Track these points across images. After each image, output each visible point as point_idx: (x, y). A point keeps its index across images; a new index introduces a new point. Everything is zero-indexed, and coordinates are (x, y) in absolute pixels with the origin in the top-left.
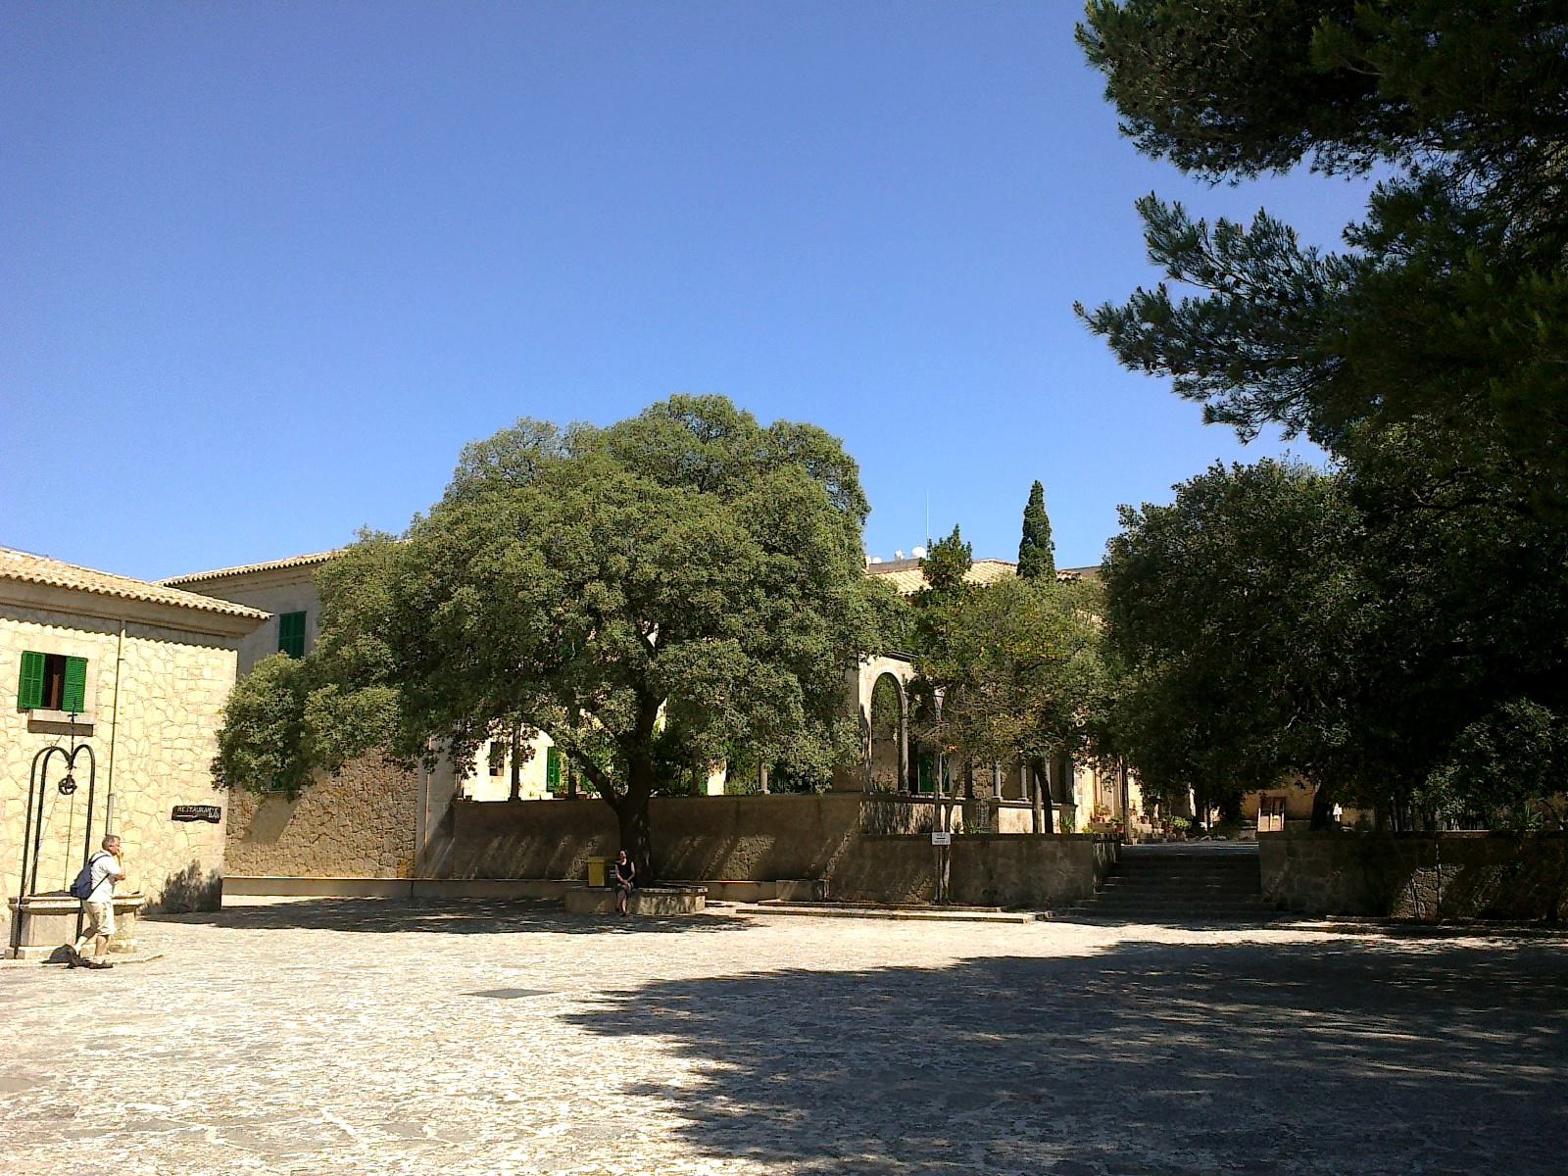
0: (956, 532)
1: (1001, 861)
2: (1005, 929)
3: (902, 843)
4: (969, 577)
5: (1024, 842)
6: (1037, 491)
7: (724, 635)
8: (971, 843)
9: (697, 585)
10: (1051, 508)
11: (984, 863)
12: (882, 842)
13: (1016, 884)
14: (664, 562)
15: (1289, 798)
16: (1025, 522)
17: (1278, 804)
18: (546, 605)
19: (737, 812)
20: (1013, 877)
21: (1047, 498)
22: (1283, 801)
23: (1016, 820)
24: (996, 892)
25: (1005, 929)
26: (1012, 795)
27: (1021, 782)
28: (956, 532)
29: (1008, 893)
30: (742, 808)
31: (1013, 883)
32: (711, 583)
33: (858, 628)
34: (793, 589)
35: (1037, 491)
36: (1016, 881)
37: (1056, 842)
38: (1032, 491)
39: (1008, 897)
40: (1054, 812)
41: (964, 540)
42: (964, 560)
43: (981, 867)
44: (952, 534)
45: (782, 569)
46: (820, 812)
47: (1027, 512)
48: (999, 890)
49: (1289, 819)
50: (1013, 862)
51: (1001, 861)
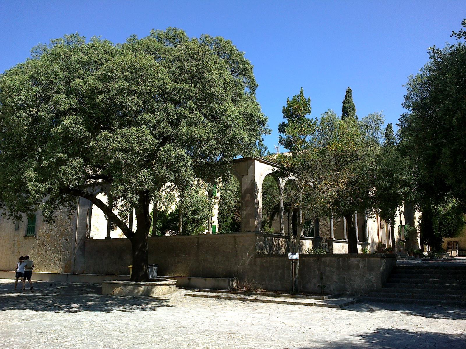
0: (301, 92)
1: (328, 269)
2: (324, 314)
3: (275, 259)
4: (307, 116)
5: (340, 259)
6: (349, 92)
7: (137, 124)
8: (312, 259)
9: (121, 91)
10: (355, 99)
11: (319, 269)
12: (265, 258)
13: (336, 282)
14: (105, 79)
15: (460, 242)
16: (343, 107)
17: (455, 244)
18: (25, 106)
19: (198, 243)
20: (335, 278)
21: (353, 95)
22: (457, 243)
23: (342, 249)
24: (324, 287)
25: (324, 314)
26: (339, 237)
27: (344, 232)
28: (301, 92)
29: (332, 287)
30: (200, 241)
31: (335, 282)
32: (132, 93)
33: (230, 126)
34: (191, 103)
35: (349, 92)
36: (336, 280)
37: (359, 259)
38: (346, 92)
39: (332, 290)
40: (358, 245)
41: (306, 96)
42: (306, 107)
43: (317, 272)
44: (299, 93)
45: (185, 92)
46: (235, 243)
47: (344, 102)
48: (327, 286)
49: (460, 250)
50: (334, 269)
51: (328, 269)
